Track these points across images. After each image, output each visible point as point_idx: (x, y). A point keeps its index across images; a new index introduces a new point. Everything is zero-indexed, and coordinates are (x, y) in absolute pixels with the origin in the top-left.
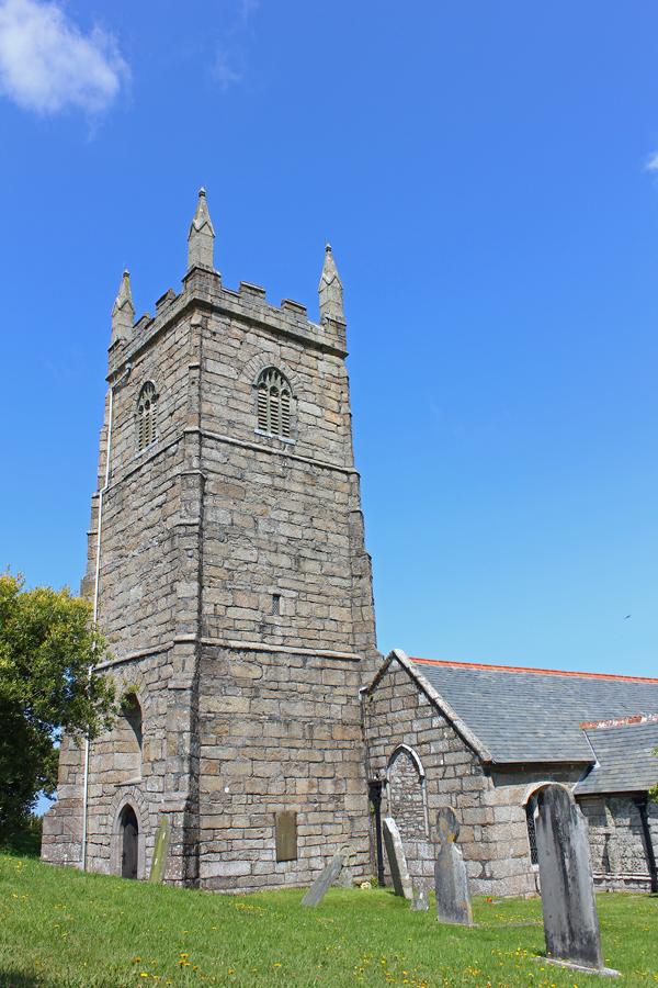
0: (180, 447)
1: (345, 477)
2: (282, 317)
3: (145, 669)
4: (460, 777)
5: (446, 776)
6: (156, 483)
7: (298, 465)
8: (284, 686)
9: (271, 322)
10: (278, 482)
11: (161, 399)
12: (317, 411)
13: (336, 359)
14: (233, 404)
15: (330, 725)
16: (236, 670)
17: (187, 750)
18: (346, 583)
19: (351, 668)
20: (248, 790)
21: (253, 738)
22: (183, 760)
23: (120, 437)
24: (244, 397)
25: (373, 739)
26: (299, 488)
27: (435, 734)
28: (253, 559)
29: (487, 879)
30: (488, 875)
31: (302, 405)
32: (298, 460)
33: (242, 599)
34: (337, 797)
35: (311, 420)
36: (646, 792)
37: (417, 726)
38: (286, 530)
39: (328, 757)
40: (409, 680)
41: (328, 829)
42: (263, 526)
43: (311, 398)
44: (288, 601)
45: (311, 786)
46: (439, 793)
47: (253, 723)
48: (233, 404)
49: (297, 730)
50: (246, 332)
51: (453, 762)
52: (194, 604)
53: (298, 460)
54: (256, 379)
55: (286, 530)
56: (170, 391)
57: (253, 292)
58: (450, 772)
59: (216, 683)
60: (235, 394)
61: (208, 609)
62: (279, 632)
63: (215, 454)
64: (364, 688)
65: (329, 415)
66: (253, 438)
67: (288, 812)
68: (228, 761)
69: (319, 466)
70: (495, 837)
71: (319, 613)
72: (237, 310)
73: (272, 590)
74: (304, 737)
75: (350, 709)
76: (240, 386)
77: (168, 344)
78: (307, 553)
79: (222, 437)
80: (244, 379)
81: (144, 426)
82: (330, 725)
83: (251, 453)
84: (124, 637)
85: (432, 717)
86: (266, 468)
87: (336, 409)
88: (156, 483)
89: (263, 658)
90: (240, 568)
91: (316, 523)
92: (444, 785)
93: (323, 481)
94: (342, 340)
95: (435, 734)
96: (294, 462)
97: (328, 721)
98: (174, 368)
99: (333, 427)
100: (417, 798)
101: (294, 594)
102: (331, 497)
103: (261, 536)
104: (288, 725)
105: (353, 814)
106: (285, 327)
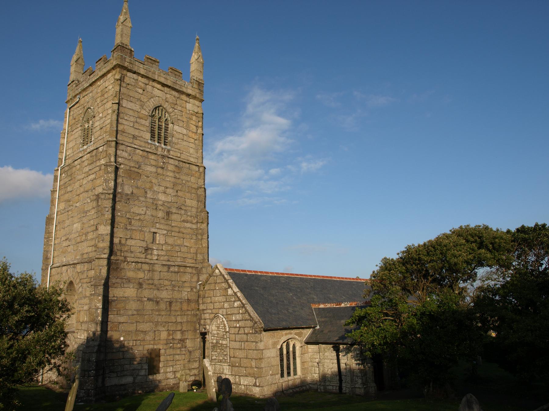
0: (105, 149)
1: (197, 168)
2: (168, 77)
3: (79, 271)
4: (247, 334)
5: (240, 332)
6: (91, 167)
7: (171, 161)
8: (156, 282)
9: (162, 80)
10: (160, 171)
11: (97, 118)
12: (185, 131)
13: (197, 103)
14: (136, 126)
15: (181, 303)
16: (130, 274)
17: (100, 318)
18: (194, 226)
19: (194, 272)
20: (134, 338)
21: (137, 310)
22: (97, 324)
23: (72, 138)
24: (143, 122)
25: (203, 310)
26: (171, 174)
27: (236, 311)
28: (143, 212)
29: (257, 386)
30: (258, 384)
31: (176, 127)
32: (172, 158)
33: (137, 235)
34: (182, 341)
35: (181, 136)
36: (333, 347)
37: (226, 305)
38: (162, 197)
39: (179, 319)
40: (223, 280)
41: (177, 357)
42: (149, 195)
43: (181, 124)
44: (161, 236)
45: (169, 335)
46: (235, 341)
47: (139, 302)
48: (136, 126)
49: (163, 306)
50: (146, 84)
51: (243, 326)
52: (108, 238)
53: (172, 158)
54: (151, 112)
55: (162, 197)
56: (101, 115)
57: (152, 62)
58: (242, 331)
59: (118, 280)
60: (138, 120)
61: (116, 240)
62: (155, 252)
63: (125, 155)
64: (200, 283)
65: (190, 134)
66: (147, 145)
67: (155, 349)
68: (123, 323)
69: (183, 162)
70: (263, 365)
71: (179, 242)
72: (142, 72)
73: (153, 230)
74: (166, 308)
75: (192, 293)
76: (141, 116)
77: (101, 88)
78: (174, 210)
79: (129, 145)
80: (143, 112)
81: (86, 132)
82: (181, 303)
83: (145, 154)
84: (69, 250)
85: (234, 301)
86: (153, 162)
87: (195, 131)
88: (91, 167)
89: (146, 267)
90: (135, 218)
91: (180, 193)
92: (238, 337)
93: (185, 171)
94: (201, 92)
95: (236, 311)
96: (170, 159)
97: (180, 300)
98: (104, 102)
99: (193, 141)
100: (224, 342)
101: (165, 232)
102: (189, 179)
103: (148, 200)
104: (158, 303)
105: (191, 349)
106: (169, 83)
